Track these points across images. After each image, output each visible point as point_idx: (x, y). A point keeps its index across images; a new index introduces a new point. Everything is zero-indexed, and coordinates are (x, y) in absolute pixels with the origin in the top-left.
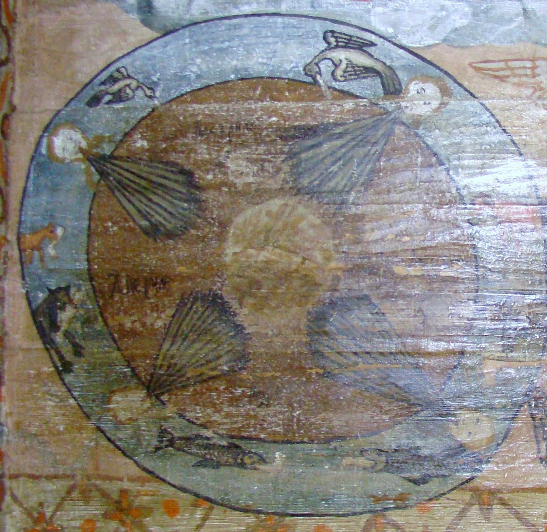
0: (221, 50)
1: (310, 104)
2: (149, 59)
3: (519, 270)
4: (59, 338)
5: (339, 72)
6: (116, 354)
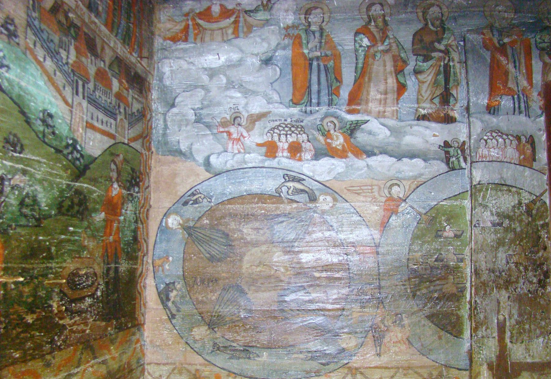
0: (240, 182)
1: (278, 205)
3: (336, 78)
4: (170, 304)
5: (290, 192)
6: (195, 311)
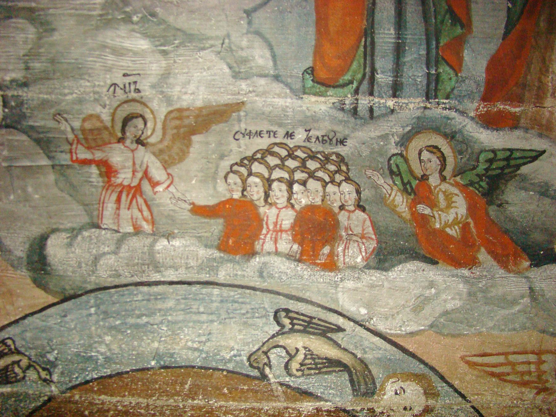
0: (137, 326)
2: (43, 331)
5: (295, 365)
